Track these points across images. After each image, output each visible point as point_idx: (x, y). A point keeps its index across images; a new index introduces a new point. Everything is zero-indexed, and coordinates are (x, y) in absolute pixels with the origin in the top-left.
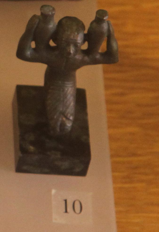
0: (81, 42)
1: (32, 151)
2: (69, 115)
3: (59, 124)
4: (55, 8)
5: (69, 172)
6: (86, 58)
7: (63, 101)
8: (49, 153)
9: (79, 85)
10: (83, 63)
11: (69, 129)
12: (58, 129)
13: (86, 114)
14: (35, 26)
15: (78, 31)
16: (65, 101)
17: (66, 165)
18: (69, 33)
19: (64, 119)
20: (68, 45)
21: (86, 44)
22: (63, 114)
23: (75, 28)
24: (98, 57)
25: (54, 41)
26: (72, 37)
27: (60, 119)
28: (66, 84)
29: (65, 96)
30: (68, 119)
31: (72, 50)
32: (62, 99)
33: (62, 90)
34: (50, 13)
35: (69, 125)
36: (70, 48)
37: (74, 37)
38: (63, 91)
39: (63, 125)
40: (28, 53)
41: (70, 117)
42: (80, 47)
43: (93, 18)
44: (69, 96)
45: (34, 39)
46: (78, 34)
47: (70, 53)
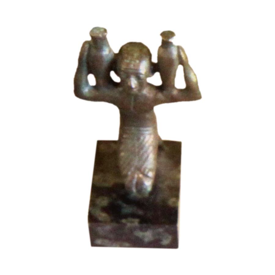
0: (146, 73)
1: (141, 236)
2: (147, 170)
3: (134, 182)
5: (156, 244)
6: (160, 96)
7: (139, 152)
8: (124, 221)
9: (166, 135)
10: (158, 102)
11: (149, 189)
12: (134, 190)
13: (179, 171)
15: (140, 59)
16: (142, 152)
17: (148, 235)
18: (128, 61)
19: (141, 176)
21: (157, 75)
22: (139, 169)
23: (136, 55)
24: (175, 93)
25: (117, 73)
26: (132, 66)
27: (136, 176)
28: (144, 131)
29: (141, 147)
30: (146, 176)
32: (137, 150)
33: (136, 138)
34: (101, 36)
35: (148, 184)
36: (130, 81)
37: (134, 66)
38: (139, 139)
39: (140, 184)
40: (86, 90)
41: (148, 172)
42: (146, 80)
43: (160, 44)
44: (151, 148)
45: (90, 72)
46: (140, 61)
47: (130, 88)
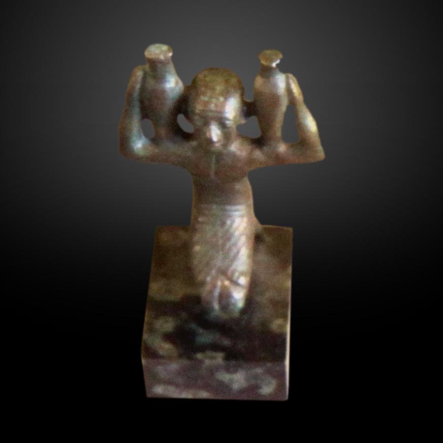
2: (237, 274)
3: (217, 293)
4: (156, 360)
7: (224, 245)
8: (199, 356)
11: (240, 304)
12: (216, 306)
14: (138, 86)
16: (228, 245)
18: (206, 99)
19: (227, 283)
20: (207, 124)
22: (224, 273)
23: (219, 88)
26: (212, 106)
27: (219, 283)
28: (231, 211)
29: (228, 236)
30: (235, 283)
31: (215, 133)
32: (220, 242)
33: (219, 222)
35: (239, 296)
36: (210, 130)
37: (216, 106)
38: (223, 224)
39: (225, 296)
41: (238, 278)
44: (243, 239)
46: (226, 99)
47: (210, 141)
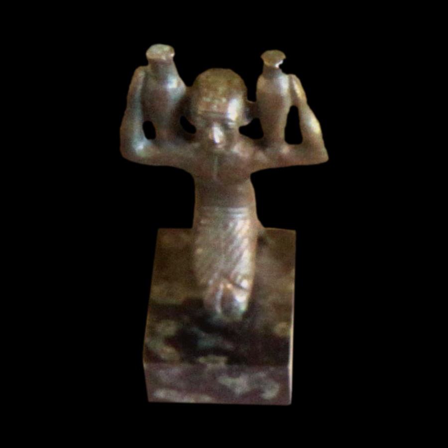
1: (229, 385)
2: (239, 277)
3: (219, 296)
7: (226, 247)
8: (202, 360)
11: (243, 308)
12: (219, 309)
16: (231, 248)
18: (208, 100)
19: (229, 286)
20: (209, 125)
22: (226, 276)
23: (221, 89)
26: (215, 108)
27: (222, 287)
28: (234, 213)
30: (238, 287)
31: (217, 135)
32: (223, 245)
33: (221, 225)
35: (241, 300)
36: (212, 132)
37: (219, 107)
38: (226, 226)
39: (228, 300)
41: (241, 281)
46: (228, 100)
47: (212, 143)
